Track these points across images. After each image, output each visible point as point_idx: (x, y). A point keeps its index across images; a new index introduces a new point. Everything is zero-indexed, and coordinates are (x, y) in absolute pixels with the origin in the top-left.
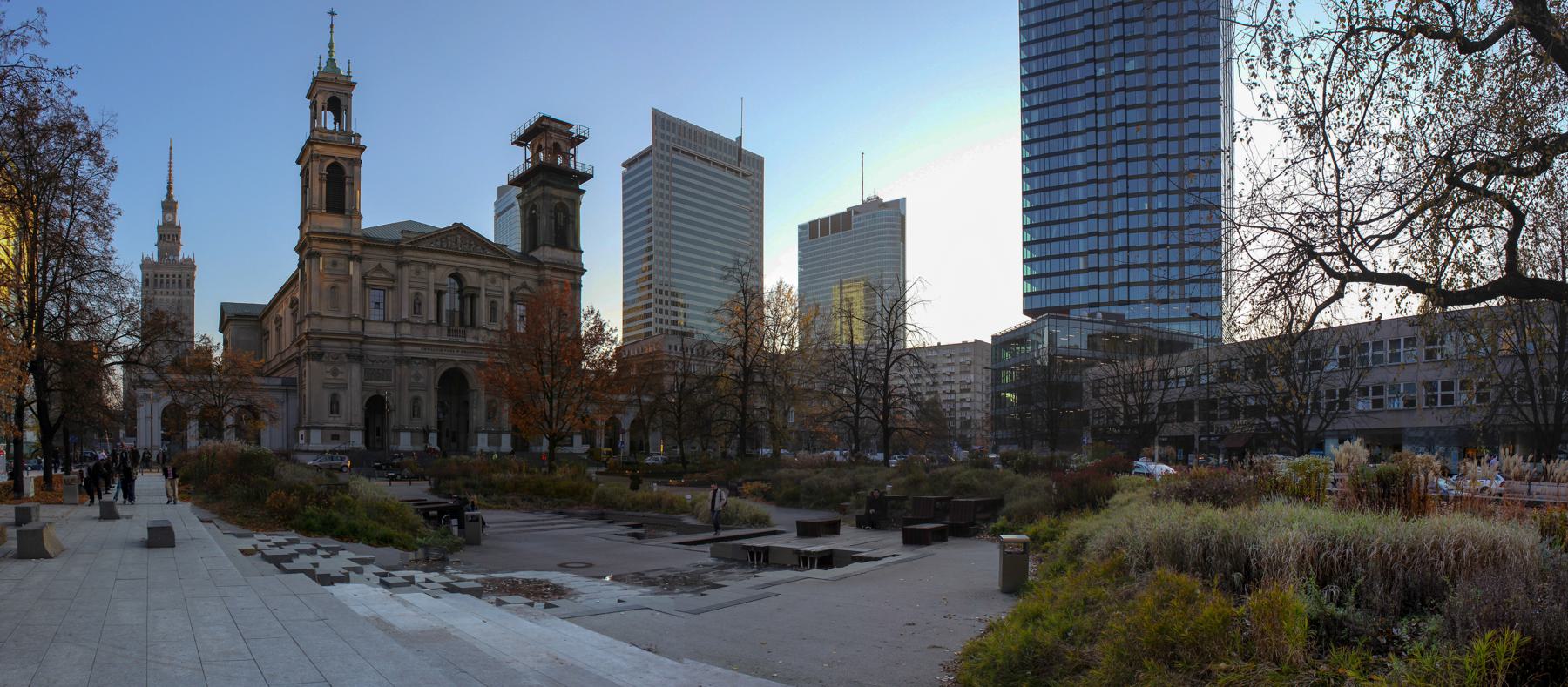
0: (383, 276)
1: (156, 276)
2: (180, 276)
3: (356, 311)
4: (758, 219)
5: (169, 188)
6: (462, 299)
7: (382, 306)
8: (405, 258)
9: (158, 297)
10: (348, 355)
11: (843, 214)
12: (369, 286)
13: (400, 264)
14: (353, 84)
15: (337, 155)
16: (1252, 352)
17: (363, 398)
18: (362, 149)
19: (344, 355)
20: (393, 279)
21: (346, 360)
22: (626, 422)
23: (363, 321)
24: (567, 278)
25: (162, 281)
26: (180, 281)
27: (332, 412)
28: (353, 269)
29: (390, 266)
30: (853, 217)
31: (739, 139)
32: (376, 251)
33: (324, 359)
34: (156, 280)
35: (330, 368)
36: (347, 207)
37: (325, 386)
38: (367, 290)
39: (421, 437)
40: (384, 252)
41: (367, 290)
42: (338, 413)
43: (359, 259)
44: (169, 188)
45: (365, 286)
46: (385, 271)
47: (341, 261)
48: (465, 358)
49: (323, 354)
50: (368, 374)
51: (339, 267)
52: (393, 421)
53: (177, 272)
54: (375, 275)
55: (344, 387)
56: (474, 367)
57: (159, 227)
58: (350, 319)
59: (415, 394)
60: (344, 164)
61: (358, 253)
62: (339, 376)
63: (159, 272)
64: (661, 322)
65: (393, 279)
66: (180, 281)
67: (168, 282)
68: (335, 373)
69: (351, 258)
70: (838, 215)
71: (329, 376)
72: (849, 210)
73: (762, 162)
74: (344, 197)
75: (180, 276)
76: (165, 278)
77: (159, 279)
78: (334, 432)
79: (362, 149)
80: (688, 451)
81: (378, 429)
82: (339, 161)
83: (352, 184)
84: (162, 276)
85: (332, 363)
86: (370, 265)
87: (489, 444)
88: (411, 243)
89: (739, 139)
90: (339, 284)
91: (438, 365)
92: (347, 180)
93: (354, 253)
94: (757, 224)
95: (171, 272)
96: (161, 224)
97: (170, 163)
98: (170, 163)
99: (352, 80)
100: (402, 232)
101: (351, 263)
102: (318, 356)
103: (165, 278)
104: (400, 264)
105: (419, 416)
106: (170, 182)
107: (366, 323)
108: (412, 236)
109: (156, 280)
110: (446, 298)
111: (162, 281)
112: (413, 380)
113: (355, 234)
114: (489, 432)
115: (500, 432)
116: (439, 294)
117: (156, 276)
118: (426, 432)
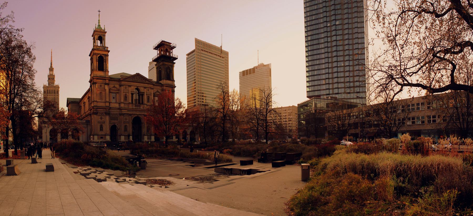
0: (115, 89)
1: (48, 90)
2: (55, 90)
5: (51, 64)
8: (122, 84)
10: (105, 113)
12: (111, 92)
18: (109, 51)
20: (118, 90)
21: (105, 114)
23: (110, 103)
25: (49, 92)
26: (55, 92)
27: (101, 130)
28: (106, 87)
29: (117, 86)
31: (221, 46)
33: (98, 114)
34: (47, 92)
35: (100, 117)
36: (104, 69)
43: (108, 84)
44: (51, 64)
45: (110, 92)
47: (103, 85)
48: (140, 113)
50: (111, 119)
51: (102, 87)
53: (54, 89)
54: (113, 89)
55: (104, 122)
57: (48, 76)
58: (106, 102)
59: (125, 124)
66: (55, 92)
68: (101, 118)
69: (106, 84)
73: (228, 54)
75: (55, 90)
77: (48, 91)
79: (109, 51)
82: (102, 55)
86: (111, 86)
88: (124, 79)
89: (221, 46)
91: (132, 116)
92: (104, 61)
93: (107, 82)
95: (52, 89)
109: (47, 92)
110: (134, 95)
111: (49, 92)
112: (125, 120)
116: (132, 94)
117: (48, 90)
118: (129, 136)
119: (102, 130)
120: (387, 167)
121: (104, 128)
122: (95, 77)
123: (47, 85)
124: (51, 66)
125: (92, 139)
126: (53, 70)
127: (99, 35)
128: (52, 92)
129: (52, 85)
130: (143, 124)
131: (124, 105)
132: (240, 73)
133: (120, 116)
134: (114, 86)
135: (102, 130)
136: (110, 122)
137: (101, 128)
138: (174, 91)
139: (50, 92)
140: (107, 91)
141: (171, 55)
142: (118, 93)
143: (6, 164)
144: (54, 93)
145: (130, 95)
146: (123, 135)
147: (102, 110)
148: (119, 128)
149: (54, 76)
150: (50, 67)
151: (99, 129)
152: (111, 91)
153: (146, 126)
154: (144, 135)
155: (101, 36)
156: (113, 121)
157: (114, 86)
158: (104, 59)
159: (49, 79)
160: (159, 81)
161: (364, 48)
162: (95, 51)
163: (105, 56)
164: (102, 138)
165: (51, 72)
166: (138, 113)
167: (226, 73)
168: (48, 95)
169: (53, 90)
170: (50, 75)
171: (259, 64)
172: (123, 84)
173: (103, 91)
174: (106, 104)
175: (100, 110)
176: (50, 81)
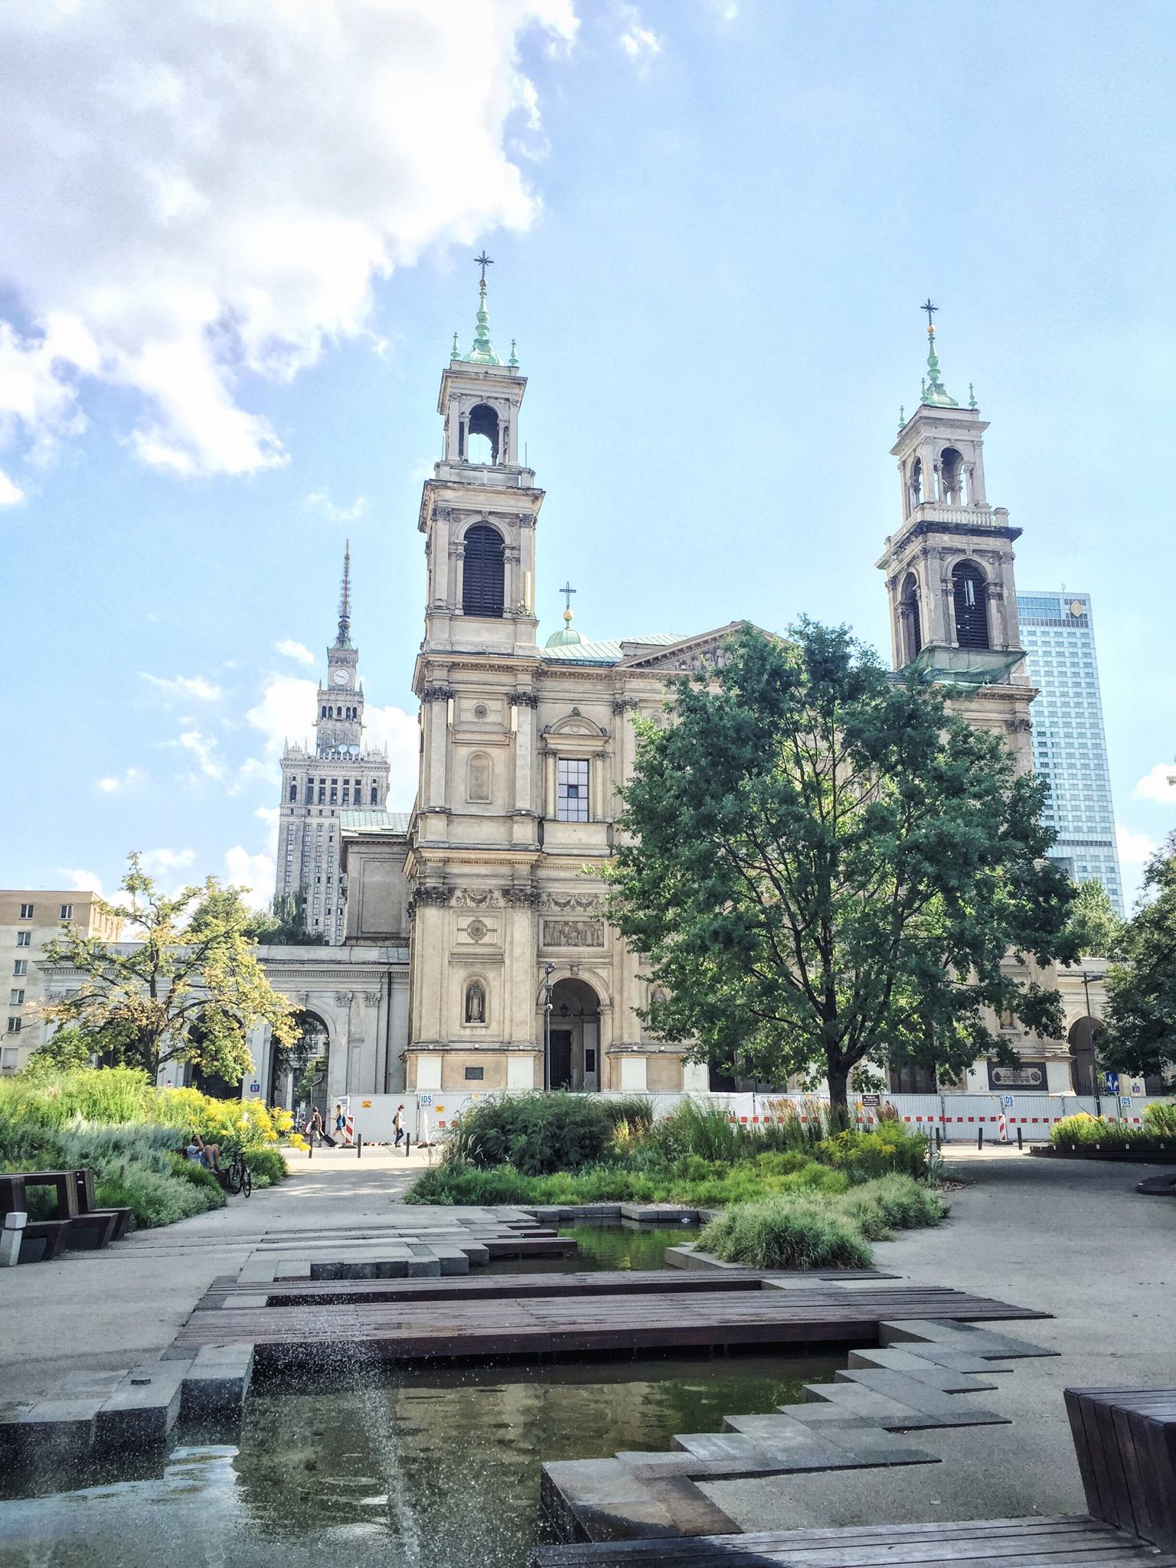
0: (583, 731)
1: (311, 781)
2: (358, 782)
3: (524, 803)
5: (344, 627)
7: (582, 791)
8: (627, 696)
9: (314, 821)
10: (506, 893)
12: (554, 753)
13: (618, 708)
14: (521, 383)
15: (486, 509)
18: (537, 496)
19: (497, 894)
20: (605, 735)
21: (502, 903)
23: (541, 821)
25: (322, 792)
26: (358, 792)
27: (469, 1019)
28: (521, 719)
29: (600, 713)
32: (568, 685)
33: (453, 902)
34: (310, 790)
35: (465, 922)
36: (507, 604)
37: (457, 958)
38: (551, 761)
40: (588, 686)
41: (551, 761)
42: (482, 1019)
43: (533, 701)
44: (344, 627)
45: (546, 753)
46: (589, 723)
47: (494, 705)
49: (451, 891)
50: (550, 934)
51: (491, 718)
52: (609, 1031)
53: (353, 776)
54: (566, 730)
55: (497, 959)
57: (321, 693)
58: (512, 816)
60: (502, 526)
61: (528, 689)
62: (486, 940)
63: (317, 774)
65: (605, 735)
66: (358, 792)
67: (334, 794)
68: (477, 931)
69: (515, 699)
71: (464, 938)
75: (358, 782)
76: (328, 785)
77: (316, 786)
78: (474, 1060)
79: (537, 496)
80: (48, 1162)
82: (492, 519)
83: (518, 560)
84: (323, 781)
85: (471, 910)
86: (553, 712)
88: (639, 665)
90: (491, 750)
92: (508, 553)
93: (521, 689)
95: (340, 775)
96: (325, 688)
97: (346, 582)
98: (346, 582)
99: (520, 374)
100: (622, 646)
101: (514, 708)
102: (442, 897)
103: (328, 785)
104: (618, 708)
106: (344, 616)
107: (546, 825)
108: (639, 652)
109: (310, 790)
111: (322, 792)
113: (521, 652)
117: (311, 781)
120: (815, 1245)
121: (494, 1004)
122: (439, 652)
123: (312, 750)
124: (342, 638)
126: (355, 661)
127: (953, 560)
128: (340, 793)
129: (342, 749)
134: (576, 713)
135: (482, 1018)
139: (328, 792)
140: (525, 742)
142: (601, 755)
143: (309, 1274)
144: (352, 799)
147: (483, 870)
148: (611, 1000)
149: (360, 694)
150: (332, 643)
151: (457, 1010)
152: (553, 743)
155: (492, 403)
156: (563, 949)
157: (576, 713)
158: (508, 541)
159: (325, 712)
162: (448, 494)
163: (512, 525)
164: (474, 1073)
165: (341, 677)
168: (315, 809)
169: (346, 782)
170: (332, 689)
172: (637, 697)
173: (494, 744)
174: (511, 833)
175: (467, 869)
176: (329, 725)
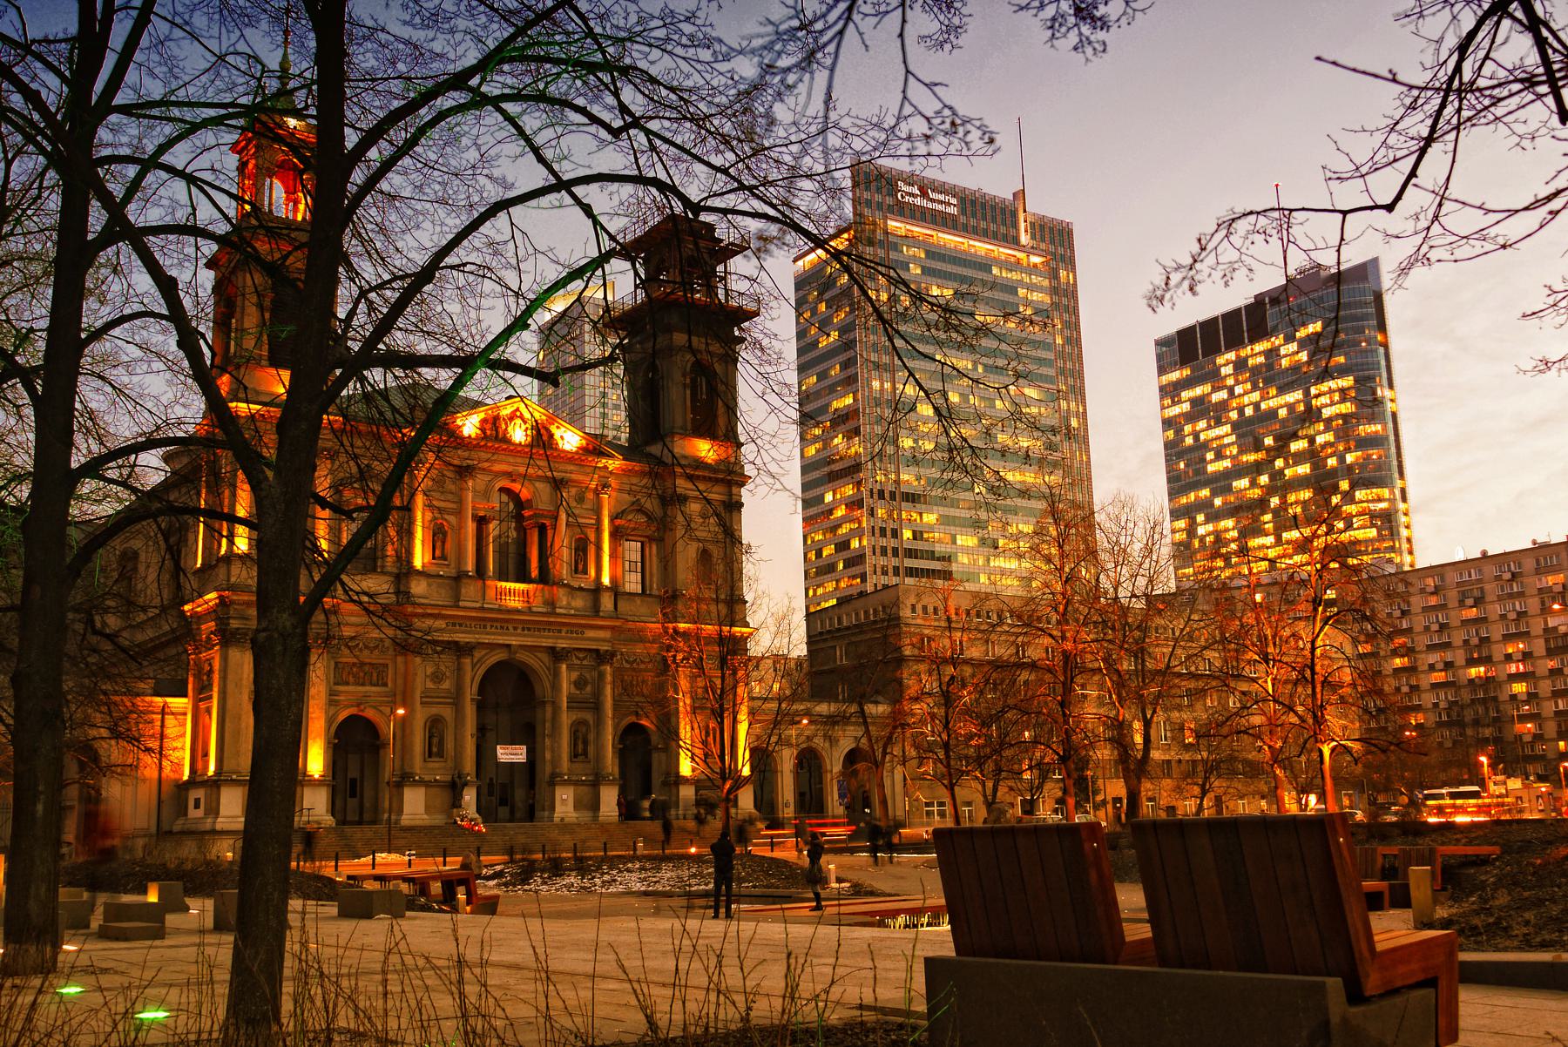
4: (1063, 257)
6: (522, 531)
11: (1246, 307)
16: (367, 831)
17: (330, 722)
22: (834, 764)
24: (716, 495)
27: (430, 756)
30: (1270, 311)
31: (1020, 195)
39: (442, 797)
48: (529, 641)
56: (545, 657)
59: (434, 710)
64: (885, 573)
70: (1237, 312)
72: (1259, 300)
73: (1070, 233)
74: (1411, 945)
81: (353, 781)
87: (576, 808)
89: (1020, 195)
91: (477, 654)
94: (1065, 301)
105: (441, 754)
110: (493, 528)
112: (430, 685)
114: (577, 783)
115: (596, 782)
116: (481, 522)
118: (455, 788)
119: (441, 754)
125: (193, 813)
130: (549, 709)
131: (429, 585)
132: (1159, 343)
133: (400, 659)
136: (332, 693)
137: (435, 740)
138: (742, 505)
141: (721, 293)
145: (471, 527)
146: (416, 784)
153: (566, 719)
154: (405, 779)
160: (647, 443)
161: (1223, 597)
166: (514, 641)
167: (1062, 372)
171: (1291, 271)
